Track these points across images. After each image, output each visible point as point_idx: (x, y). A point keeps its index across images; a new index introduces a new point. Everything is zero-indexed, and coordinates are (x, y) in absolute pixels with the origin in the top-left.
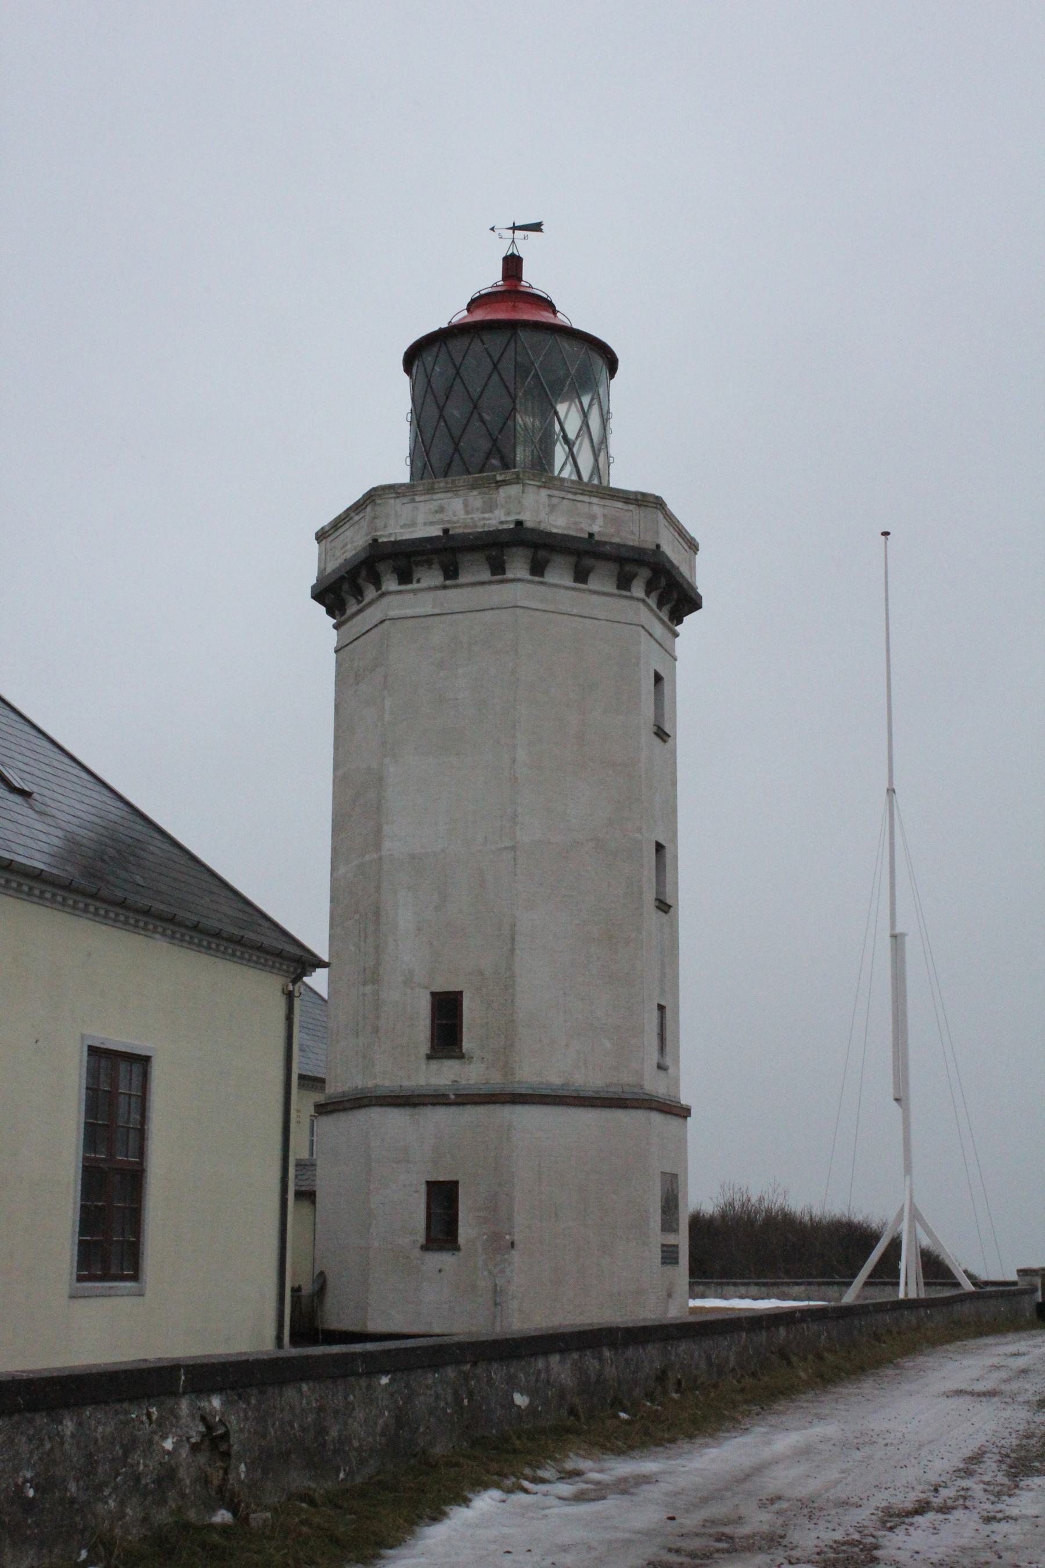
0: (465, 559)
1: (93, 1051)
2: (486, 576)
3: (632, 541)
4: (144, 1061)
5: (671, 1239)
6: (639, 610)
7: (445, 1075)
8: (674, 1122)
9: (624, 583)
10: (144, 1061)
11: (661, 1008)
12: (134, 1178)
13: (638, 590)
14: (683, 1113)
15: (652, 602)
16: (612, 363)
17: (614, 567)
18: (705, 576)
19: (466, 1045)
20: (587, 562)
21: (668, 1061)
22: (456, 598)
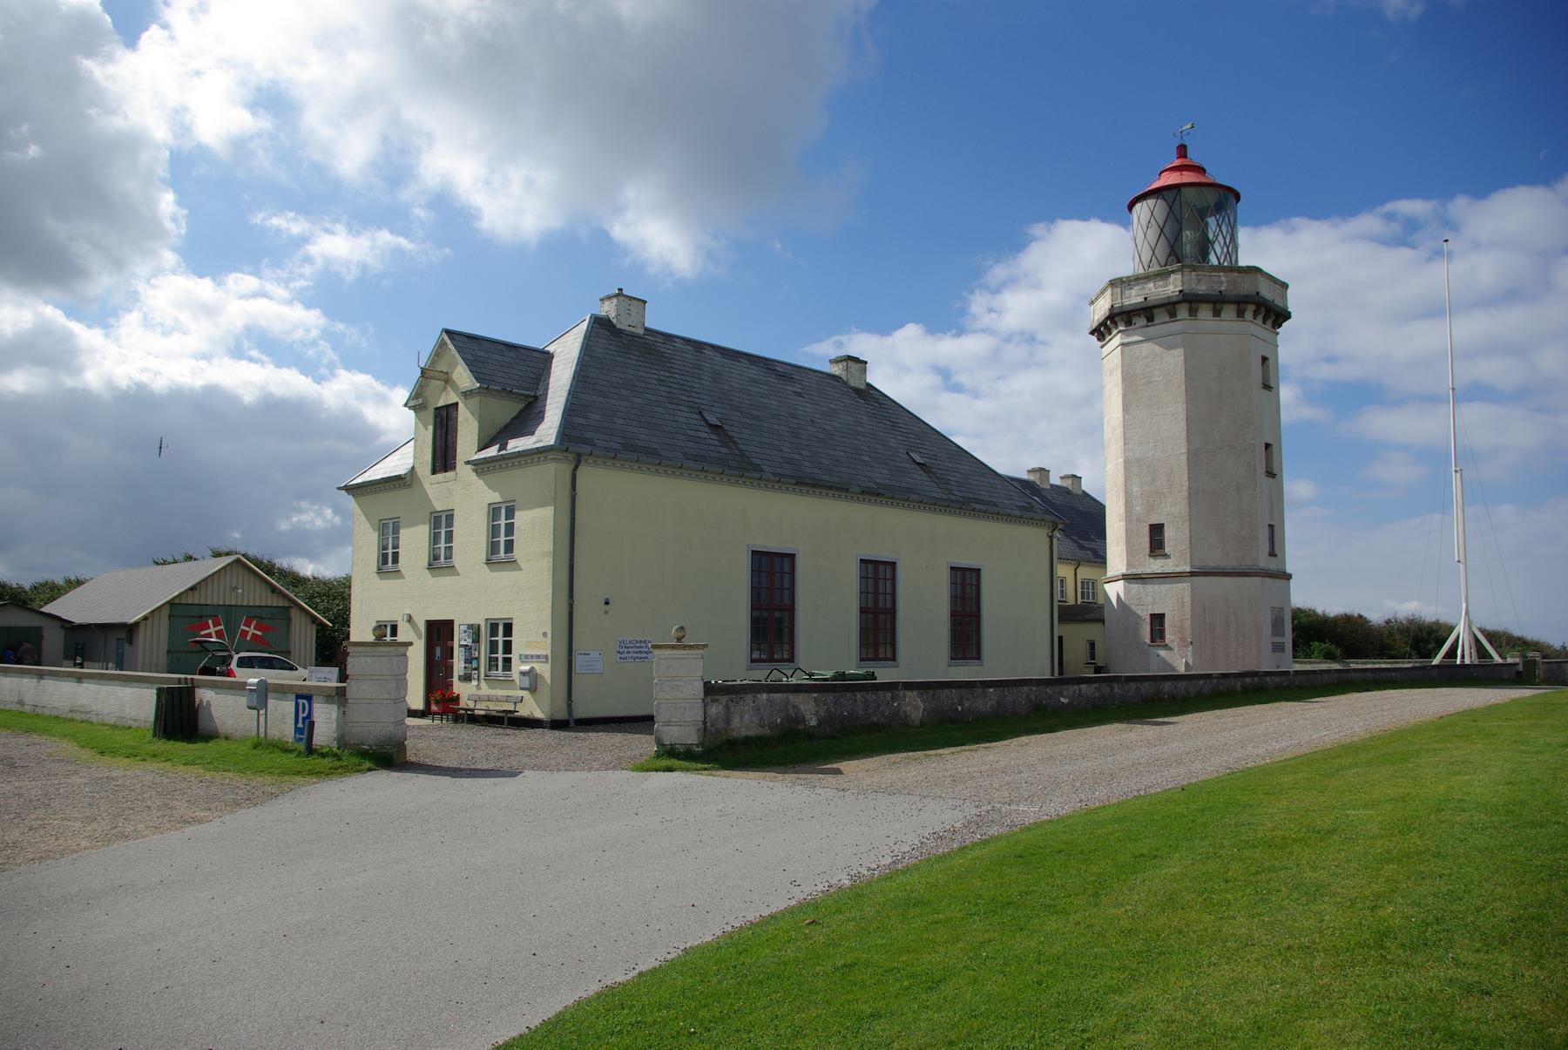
0: (1155, 311)
1: (862, 561)
2: (1167, 318)
3: (1243, 292)
4: (792, 557)
5: (1278, 640)
6: (1253, 327)
7: (1157, 566)
8: (1281, 582)
9: (1240, 314)
10: (792, 557)
11: (1271, 526)
12: (976, 616)
13: (1249, 315)
14: (1289, 577)
15: (1259, 320)
16: (1237, 197)
17: (1210, 306)
18: (1293, 303)
19: (1167, 550)
20: (1218, 306)
21: (1277, 551)
22: (1238, 325)
